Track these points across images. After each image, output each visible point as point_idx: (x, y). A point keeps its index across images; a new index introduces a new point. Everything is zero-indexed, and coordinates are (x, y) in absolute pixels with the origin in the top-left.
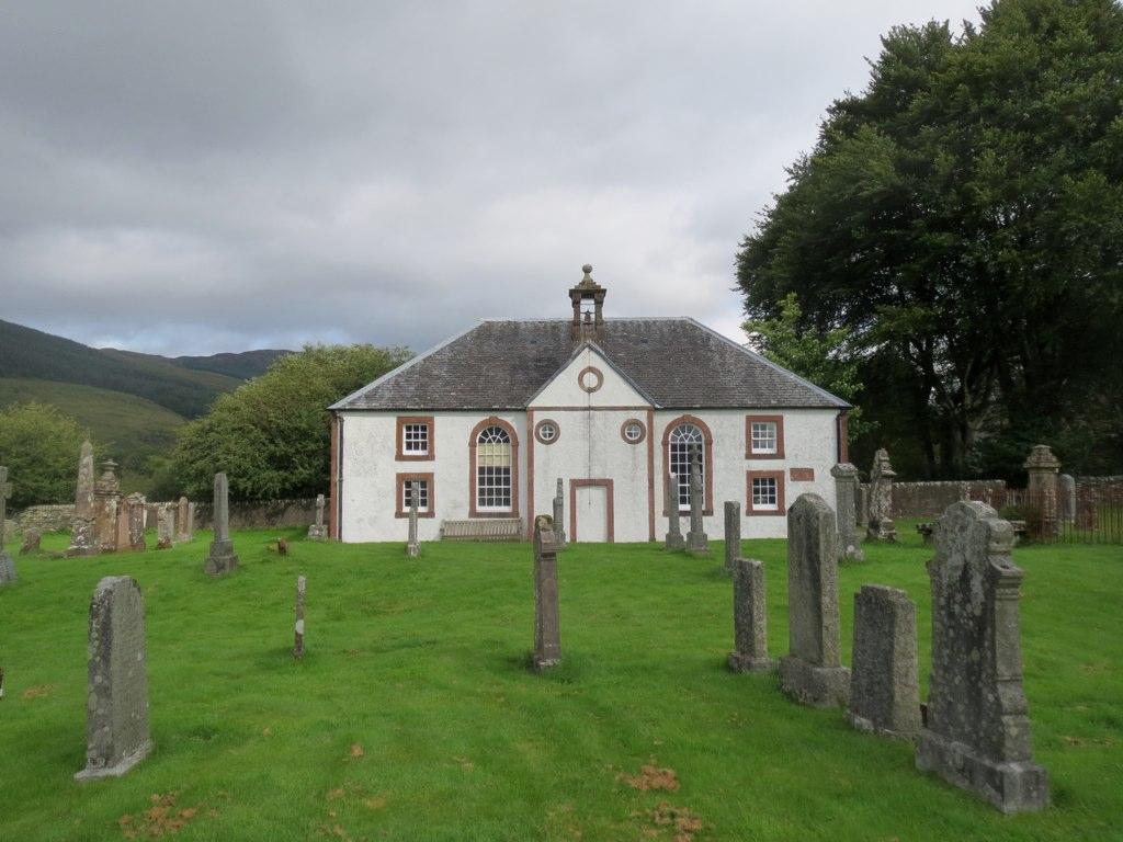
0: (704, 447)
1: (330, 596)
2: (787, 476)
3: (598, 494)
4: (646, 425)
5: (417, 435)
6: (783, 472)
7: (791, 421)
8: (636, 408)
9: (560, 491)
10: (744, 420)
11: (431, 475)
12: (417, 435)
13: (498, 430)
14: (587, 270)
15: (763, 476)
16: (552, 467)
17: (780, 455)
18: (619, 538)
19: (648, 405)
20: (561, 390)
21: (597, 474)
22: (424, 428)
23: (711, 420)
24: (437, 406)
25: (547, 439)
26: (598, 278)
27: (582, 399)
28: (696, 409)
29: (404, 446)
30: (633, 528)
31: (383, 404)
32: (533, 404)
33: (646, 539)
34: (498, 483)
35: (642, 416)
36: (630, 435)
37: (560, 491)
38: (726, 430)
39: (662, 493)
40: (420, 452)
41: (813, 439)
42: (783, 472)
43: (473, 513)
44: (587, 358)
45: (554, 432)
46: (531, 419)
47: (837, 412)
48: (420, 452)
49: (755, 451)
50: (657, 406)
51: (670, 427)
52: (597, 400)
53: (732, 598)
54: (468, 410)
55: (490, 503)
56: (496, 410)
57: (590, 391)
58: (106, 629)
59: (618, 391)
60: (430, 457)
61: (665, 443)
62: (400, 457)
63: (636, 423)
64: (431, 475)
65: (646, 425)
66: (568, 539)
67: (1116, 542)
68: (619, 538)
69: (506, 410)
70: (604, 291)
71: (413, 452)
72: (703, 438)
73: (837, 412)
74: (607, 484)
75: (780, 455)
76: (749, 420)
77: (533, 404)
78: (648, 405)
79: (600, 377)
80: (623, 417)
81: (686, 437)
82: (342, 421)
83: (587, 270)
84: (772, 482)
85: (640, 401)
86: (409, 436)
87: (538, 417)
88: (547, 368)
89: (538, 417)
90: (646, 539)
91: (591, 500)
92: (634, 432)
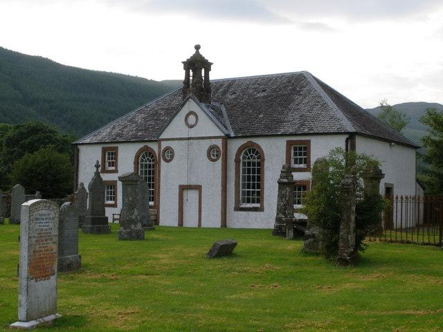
8: (215, 138)
10: (101, 151)
13: (254, 150)
14: (197, 47)
18: (204, 225)
20: (177, 128)
21: (193, 182)
22: (305, 149)
23: (263, 143)
27: (186, 132)
29: (293, 161)
32: (162, 137)
34: (253, 192)
35: (219, 143)
39: (118, 190)
40: (302, 166)
46: (160, 147)
47: (347, 136)
48: (302, 166)
51: (240, 150)
52: (193, 133)
53: (79, 243)
54: (133, 142)
56: (145, 141)
57: (191, 127)
59: (208, 127)
61: (237, 161)
67: (440, 245)
68: (204, 225)
69: (153, 141)
71: (297, 166)
73: (347, 136)
74: (198, 188)
76: (289, 144)
77: (162, 137)
80: (206, 144)
83: (197, 47)
86: (295, 154)
87: (164, 145)
88: (172, 112)
89: (164, 145)
90: (196, 225)
92: (213, 154)
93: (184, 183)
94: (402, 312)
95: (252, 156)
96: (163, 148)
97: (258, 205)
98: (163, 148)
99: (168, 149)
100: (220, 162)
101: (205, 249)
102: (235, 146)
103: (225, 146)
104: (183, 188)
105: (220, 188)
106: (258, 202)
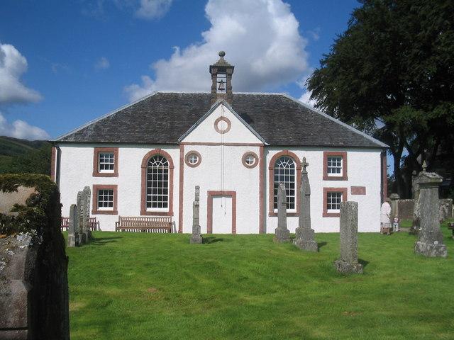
0: (296, 171)
1: (314, 260)
2: (349, 192)
3: (230, 200)
4: (259, 156)
5: (104, 162)
6: (325, 189)
7: (353, 157)
9: (197, 195)
11: (116, 186)
12: (104, 162)
14: (222, 54)
15: (107, 188)
16: (190, 183)
17: (345, 178)
18: (238, 232)
19: (261, 142)
20: (203, 131)
21: (227, 189)
23: (300, 154)
24: (349, 144)
25: (193, 164)
26: (228, 59)
27: (217, 138)
28: (117, 143)
30: (248, 225)
31: (86, 139)
33: (256, 231)
34: (155, 192)
35: (257, 150)
36: (195, 161)
37: (197, 195)
38: (314, 160)
41: (366, 168)
42: (325, 189)
43: (143, 212)
44: (223, 111)
45: (198, 159)
46: (182, 151)
49: (330, 175)
50: (266, 144)
52: (227, 138)
55: (155, 206)
58: (343, 275)
60: (116, 175)
62: (326, 178)
63: (252, 155)
64: (116, 186)
65: (259, 156)
66: (177, 230)
69: (168, 144)
70: (233, 68)
72: (296, 166)
74: (232, 195)
75: (345, 178)
78: (261, 142)
79: (229, 123)
80: (243, 151)
81: (158, 163)
82: (59, 151)
83: (222, 54)
84: (111, 192)
85: (254, 139)
87: (187, 149)
89: (187, 149)
90: (256, 231)
91: (222, 205)
93: (217, 188)
94: (369, 302)
95: (284, 164)
96: (186, 152)
97: (166, 210)
98: (186, 152)
99: (194, 155)
100: (258, 168)
101: (327, 245)
102: (272, 153)
103: (264, 154)
104: (213, 195)
105: (258, 195)
106: (111, 205)
